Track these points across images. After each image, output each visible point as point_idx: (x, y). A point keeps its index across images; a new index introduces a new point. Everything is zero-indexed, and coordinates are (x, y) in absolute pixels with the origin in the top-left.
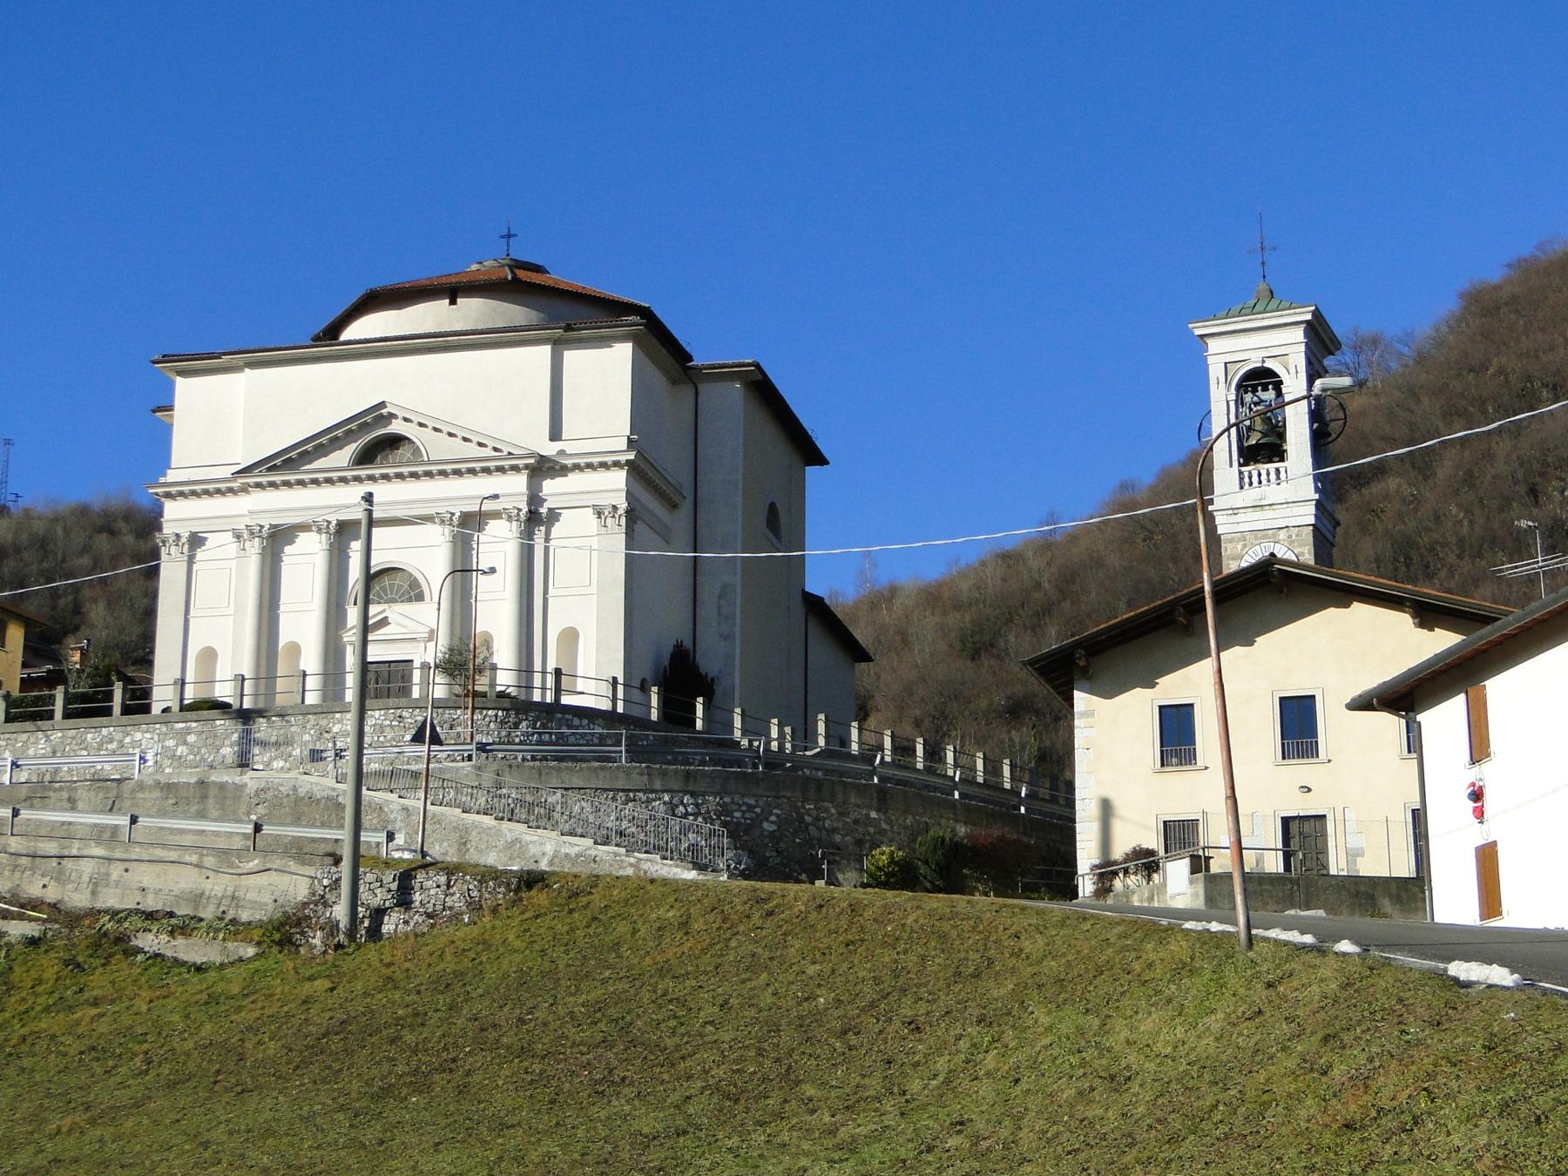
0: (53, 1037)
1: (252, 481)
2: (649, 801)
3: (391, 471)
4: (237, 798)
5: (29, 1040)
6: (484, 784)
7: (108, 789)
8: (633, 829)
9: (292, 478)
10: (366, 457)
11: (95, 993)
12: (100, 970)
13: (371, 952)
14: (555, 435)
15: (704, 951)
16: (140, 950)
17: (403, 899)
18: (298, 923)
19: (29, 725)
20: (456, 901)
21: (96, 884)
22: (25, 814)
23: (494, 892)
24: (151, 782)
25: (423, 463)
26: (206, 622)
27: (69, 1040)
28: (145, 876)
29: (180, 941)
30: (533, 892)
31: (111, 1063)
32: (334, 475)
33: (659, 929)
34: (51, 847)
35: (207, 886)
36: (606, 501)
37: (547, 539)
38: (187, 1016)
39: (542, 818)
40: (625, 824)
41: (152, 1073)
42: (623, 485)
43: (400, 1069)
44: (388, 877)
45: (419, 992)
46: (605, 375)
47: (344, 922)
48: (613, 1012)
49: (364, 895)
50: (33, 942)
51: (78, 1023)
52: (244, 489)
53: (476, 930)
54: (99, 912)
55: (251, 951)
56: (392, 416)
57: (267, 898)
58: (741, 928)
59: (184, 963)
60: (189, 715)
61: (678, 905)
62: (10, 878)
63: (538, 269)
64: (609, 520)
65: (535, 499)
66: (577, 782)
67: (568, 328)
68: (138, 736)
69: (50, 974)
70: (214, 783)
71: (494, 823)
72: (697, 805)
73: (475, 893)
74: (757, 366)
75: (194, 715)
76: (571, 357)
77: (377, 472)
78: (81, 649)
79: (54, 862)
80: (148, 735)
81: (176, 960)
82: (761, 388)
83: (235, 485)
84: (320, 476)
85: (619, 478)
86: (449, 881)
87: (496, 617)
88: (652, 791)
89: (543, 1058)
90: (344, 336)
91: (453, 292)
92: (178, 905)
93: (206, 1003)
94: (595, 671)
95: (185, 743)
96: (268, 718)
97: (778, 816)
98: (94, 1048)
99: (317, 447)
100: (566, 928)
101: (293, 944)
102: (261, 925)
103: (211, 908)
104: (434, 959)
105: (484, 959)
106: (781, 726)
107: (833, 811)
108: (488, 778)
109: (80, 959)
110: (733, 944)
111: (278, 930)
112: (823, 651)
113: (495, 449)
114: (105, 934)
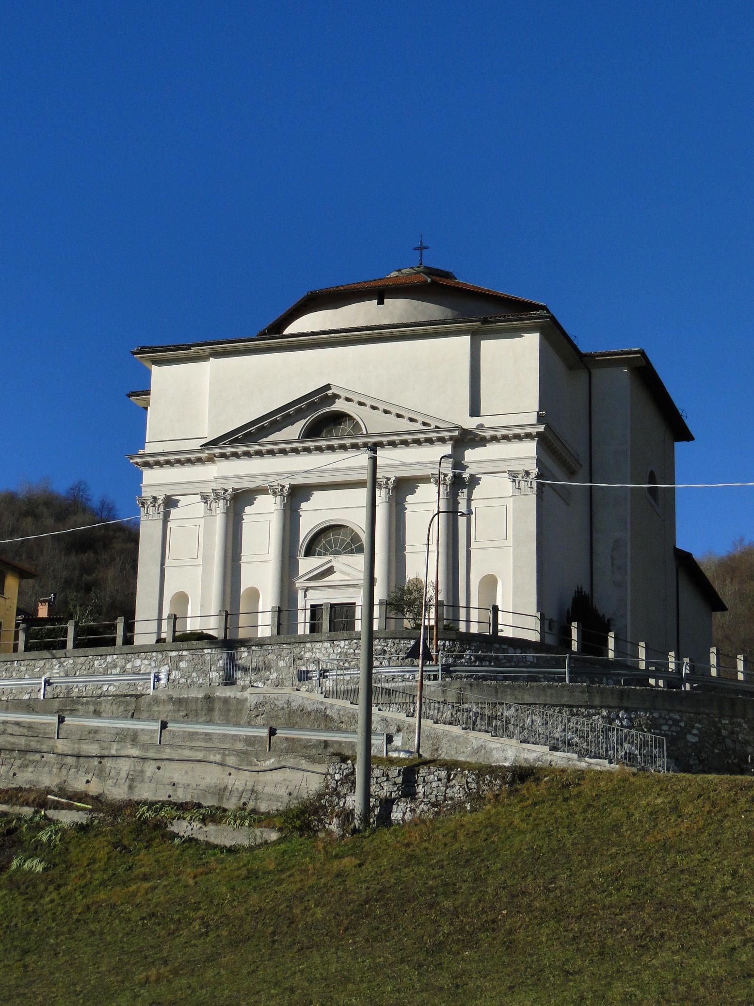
0: (114, 906)
1: (217, 451)
2: (589, 716)
3: (335, 443)
4: (239, 711)
5: (93, 908)
6: (449, 700)
7: (128, 704)
8: (577, 739)
9: (251, 449)
10: (312, 432)
11: (143, 870)
12: (143, 852)
13: (386, 835)
14: (475, 411)
15: (701, 831)
16: (177, 835)
17: (408, 790)
18: (316, 812)
19: (45, 654)
20: (456, 792)
21: (132, 781)
22: (69, 720)
23: (491, 785)
24: (165, 697)
25: (362, 436)
26: (180, 571)
27: (129, 908)
28: (175, 772)
29: (211, 828)
30: (527, 783)
31: (172, 926)
32: (288, 446)
33: (652, 813)
34: (93, 749)
35: (230, 781)
36: (520, 467)
37: (469, 500)
38: (233, 888)
39: (501, 729)
40: (569, 735)
41: (212, 935)
42: (533, 453)
43: (446, 929)
44: (394, 772)
45: (442, 867)
46: (515, 364)
47: (358, 810)
48: (632, 880)
49: (373, 789)
50: (82, 828)
51: (134, 894)
52: (211, 459)
53: (481, 816)
54: (138, 803)
55: (274, 836)
56: (336, 396)
57: (282, 792)
58: (730, 811)
59: (216, 846)
60: (180, 645)
61: (664, 793)
62: (58, 775)
63: (448, 275)
64: (523, 484)
65: (459, 465)
66: (528, 699)
67: (485, 321)
68: (138, 662)
69: (102, 854)
70: (219, 698)
71: (461, 732)
72: (630, 719)
73: (473, 785)
74: (643, 353)
75: (185, 645)
76: (488, 346)
77: (323, 444)
78: (49, 601)
79: (96, 762)
80: (146, 662)
81: (207, 843)
82: (644, 374)
83: (203, 455)
84: (276, 447)
85: (530, 448)
86: (449, 775)
87: (423, 565)
88: (592, 707)
89: (579, 918)
90: (288, 331)
91: (380, 294)
92: (205, 797)
93: (247, 878)
94: (518, 614)
95: (178, 668)
96: (249, 647)
97: (698, 729)
98: (153, 915)
99: (285, 417)
100: (565, 813)
101: (312, 829)
102: (280, 814)
103: (234, 800)
104: (448, 840)
105: (496, 839)
106: (678, 658)
107: (745, 726)
108: (452, 695)
109: (126, 842)
110: (727, 824)
111: (298, 818)
112: (690, 600)
113: (424, 424)
114: (145, 822)
